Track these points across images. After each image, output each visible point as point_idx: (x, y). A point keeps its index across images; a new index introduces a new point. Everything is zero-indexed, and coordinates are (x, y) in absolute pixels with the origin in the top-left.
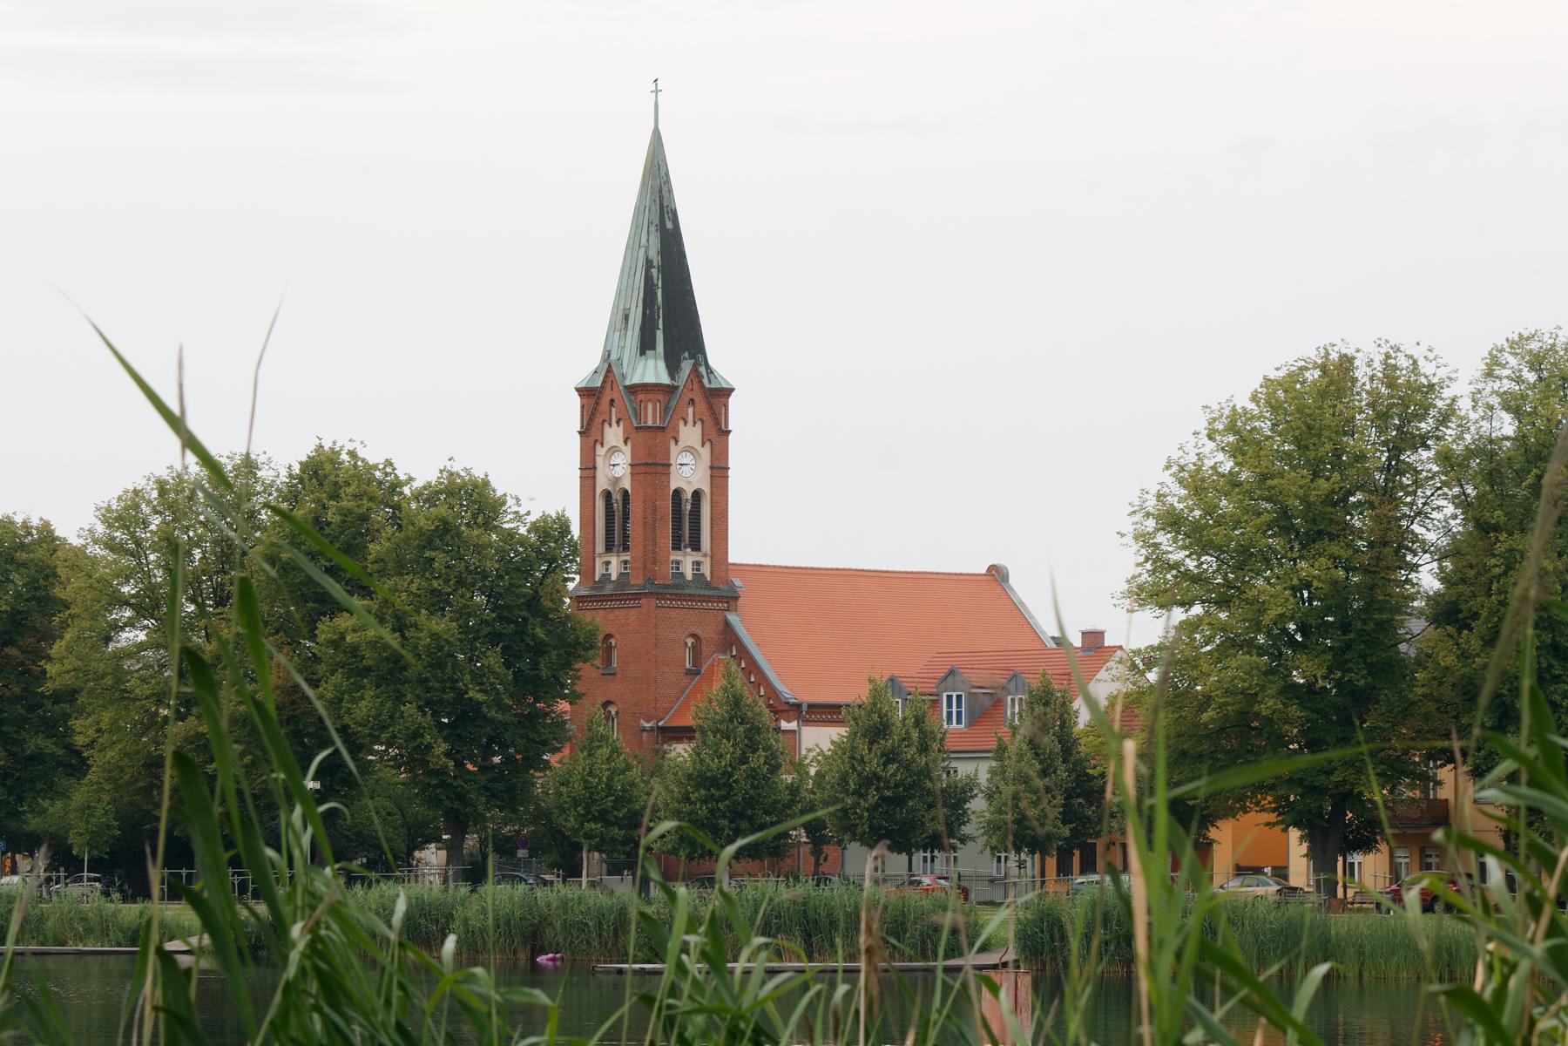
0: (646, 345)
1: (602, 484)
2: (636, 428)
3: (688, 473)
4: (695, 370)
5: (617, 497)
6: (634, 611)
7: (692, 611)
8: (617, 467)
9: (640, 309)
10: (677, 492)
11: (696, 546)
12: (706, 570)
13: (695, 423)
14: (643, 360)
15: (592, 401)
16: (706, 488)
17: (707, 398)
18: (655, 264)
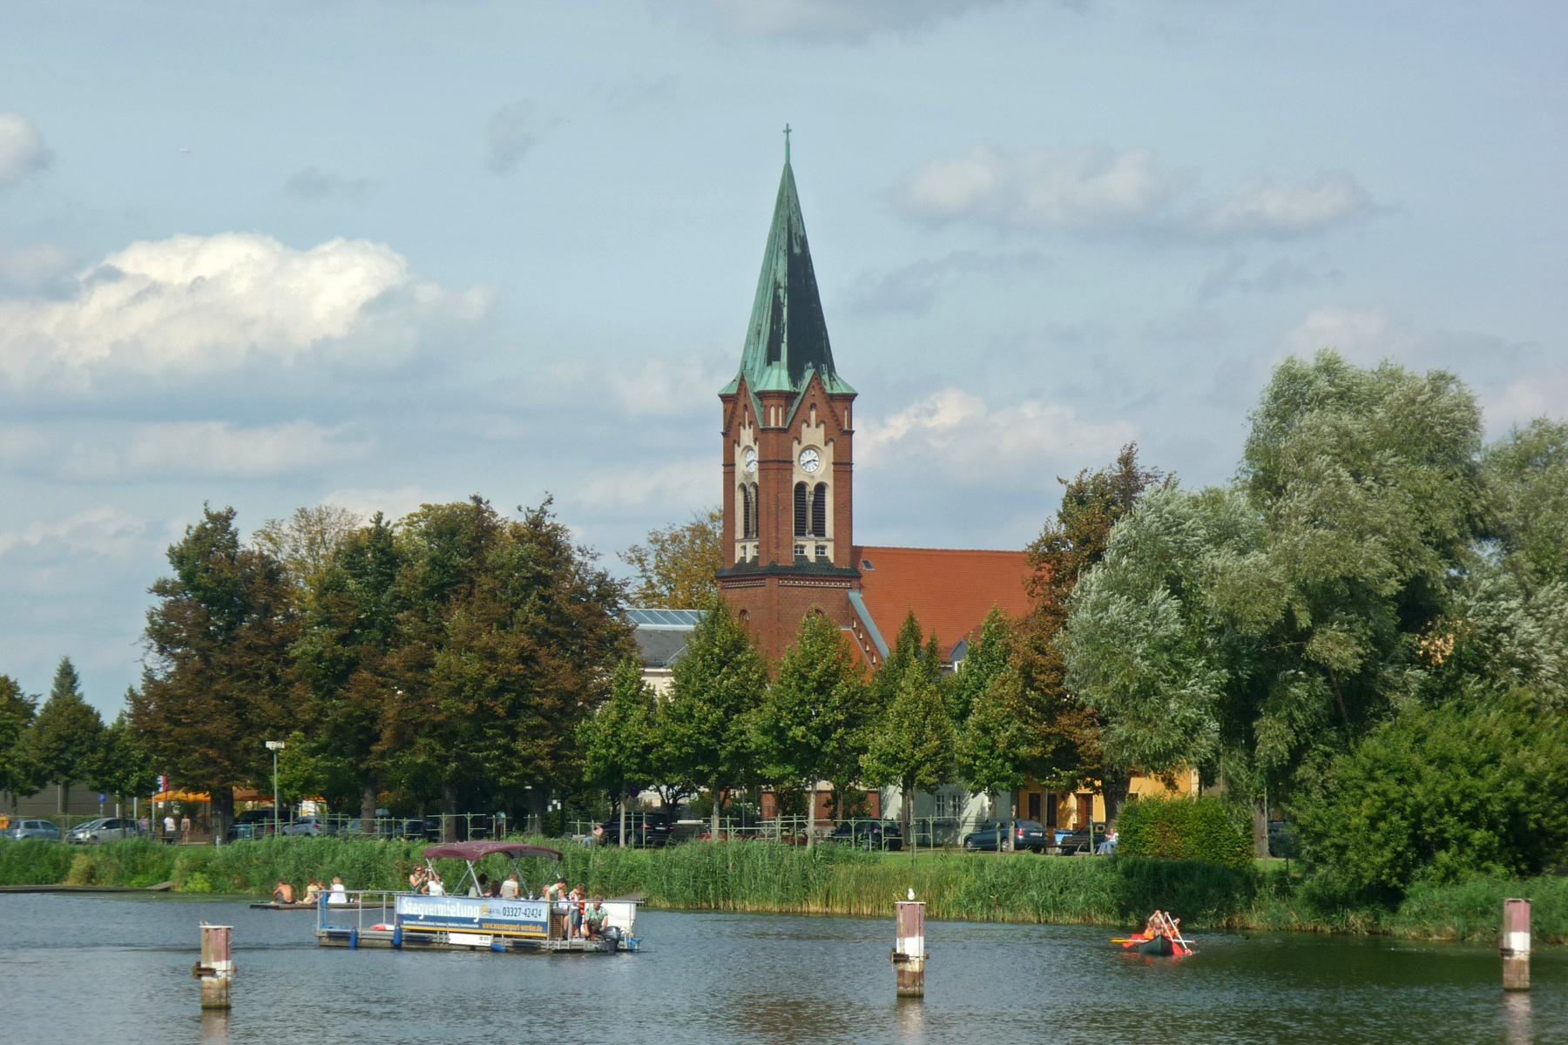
0: (772, 356)
1: (739, 479)
2: (762, 430)
3: (813, 466)
4: (817, 378)
5: (811, 488)
6: (761, 589)
7: (814, 589)
8: (748, 464)
9: (769, 325)
10: (801, 487)
11: (819, 531)
12: (830, 553)
13: (817, 426)
14: (769, 370)
15: (731, 406)
16: (830, 482)
17: (827, 402)
18: (782, 285)
